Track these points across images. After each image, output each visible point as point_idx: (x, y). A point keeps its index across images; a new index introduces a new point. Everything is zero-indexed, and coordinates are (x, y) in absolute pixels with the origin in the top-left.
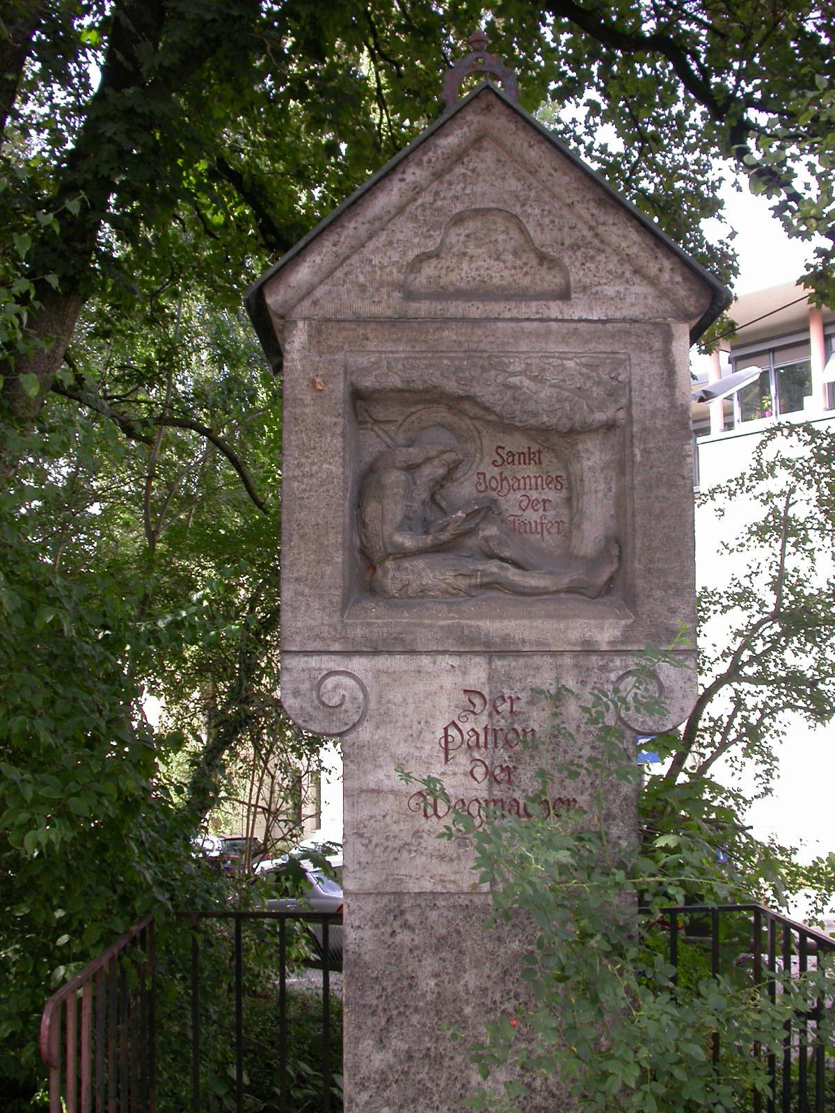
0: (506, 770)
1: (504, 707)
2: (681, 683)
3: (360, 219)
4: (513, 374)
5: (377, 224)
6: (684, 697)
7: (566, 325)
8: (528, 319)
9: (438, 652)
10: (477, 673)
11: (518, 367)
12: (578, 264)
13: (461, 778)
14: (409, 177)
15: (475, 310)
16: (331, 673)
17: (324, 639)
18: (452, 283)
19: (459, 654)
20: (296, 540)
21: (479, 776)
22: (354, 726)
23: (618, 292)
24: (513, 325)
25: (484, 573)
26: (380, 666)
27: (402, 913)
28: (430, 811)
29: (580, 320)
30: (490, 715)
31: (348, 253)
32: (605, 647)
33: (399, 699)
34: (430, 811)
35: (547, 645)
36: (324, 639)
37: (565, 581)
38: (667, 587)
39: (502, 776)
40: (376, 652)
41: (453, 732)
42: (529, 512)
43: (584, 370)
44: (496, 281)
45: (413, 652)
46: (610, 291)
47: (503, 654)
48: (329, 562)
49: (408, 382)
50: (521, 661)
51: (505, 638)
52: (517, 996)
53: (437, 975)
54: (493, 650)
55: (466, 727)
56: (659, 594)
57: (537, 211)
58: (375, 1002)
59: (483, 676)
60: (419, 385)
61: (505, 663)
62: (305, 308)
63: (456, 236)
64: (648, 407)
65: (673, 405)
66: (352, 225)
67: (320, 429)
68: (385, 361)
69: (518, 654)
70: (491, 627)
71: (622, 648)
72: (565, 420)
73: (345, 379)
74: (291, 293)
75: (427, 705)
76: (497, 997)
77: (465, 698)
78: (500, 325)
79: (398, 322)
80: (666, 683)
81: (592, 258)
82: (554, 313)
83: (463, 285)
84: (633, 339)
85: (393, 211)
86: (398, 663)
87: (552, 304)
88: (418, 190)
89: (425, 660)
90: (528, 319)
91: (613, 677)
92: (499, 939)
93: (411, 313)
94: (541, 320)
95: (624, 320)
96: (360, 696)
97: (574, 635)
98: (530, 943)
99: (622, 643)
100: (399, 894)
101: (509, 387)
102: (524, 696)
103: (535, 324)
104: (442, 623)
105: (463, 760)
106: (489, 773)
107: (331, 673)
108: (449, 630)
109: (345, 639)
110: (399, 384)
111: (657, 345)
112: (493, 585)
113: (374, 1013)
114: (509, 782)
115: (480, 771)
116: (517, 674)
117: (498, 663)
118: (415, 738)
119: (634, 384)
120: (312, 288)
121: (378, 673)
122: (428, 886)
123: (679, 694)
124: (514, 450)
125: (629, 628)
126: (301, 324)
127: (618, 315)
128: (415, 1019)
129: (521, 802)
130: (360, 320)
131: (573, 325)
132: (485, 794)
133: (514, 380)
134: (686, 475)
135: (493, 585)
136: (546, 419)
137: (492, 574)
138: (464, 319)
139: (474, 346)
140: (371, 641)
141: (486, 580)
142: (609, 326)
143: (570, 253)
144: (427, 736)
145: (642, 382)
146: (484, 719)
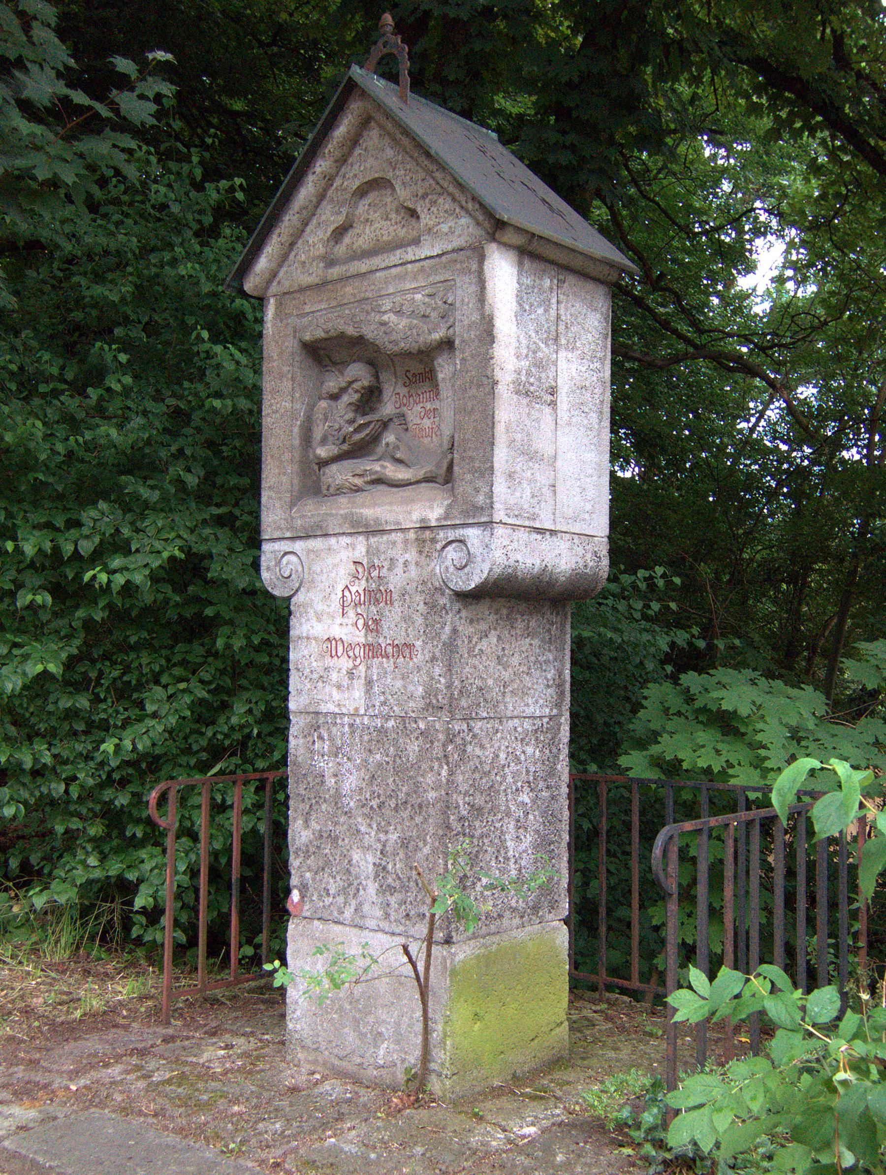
0: (376, 622)
1: (375, 574)
2: (481, 550)
3: (291, 212)
4: (385, 312)
5: (305, 212)
6: (483, 561)
7: (417, 264)
8: (395, 266)
9: (340, 534)
10: (360, 547)
11: (387, 306)
12: (426, 211)
13: (350, 627)
14: (318, 170)
15: (363, 266)
16: (286, 553)
17: (282, 529)
18: (360, 247)
19: (351, 534)
20: (269, 460)
21: (360, 627)
22: (297, 591)
23: (450, 227)
24: (385, 272)
25: (372, 472)
26: (310, 547)
27: (319, 727)
28: (334, 653)
29: (426, 258)
30: (367, 580)
31: (290, 240)
32: (434, 524)
33: (319, 570)
34: (334, 653)
35: (398, 523)
36: (282, 529)
37: (421, 474)
38: (473, 471)
39: (373, 626)
40: (308, 537)
41: (347, 593)
42: (426, 420)
43: (427, 300)
44: (385, 238)
45: (326, 535)
46: (445, 228)
47: (375, 533)
48: (285, 474)
49: (327, 332)
50: (385, 538)
51: (377, 520)
52: (379, 796)
53: (336, 775)
54: (372, 530)
55: (353, 589)
56: (468, 477)
57: (402, 172)
58: (304, 792)
59: (364, 550)
60: (332, 333)
61: (376, 539)
62: (274, 288)
63: (362, 207)
64: (466, 322)
65: (483, 315)
66: (287, 218)
67: (281, 376)
68: (320, 319)
69: (383, 532)
70: (369, 513)
71: (445, 523)
72: (414, 344)
73: (295, 337)
74: (258, 279)
75: (333, 575)
76: (368, 796)
77: (353, 567)
78: (378, 274)
79: (322, 285)
80: (472, 550)
81: (435, 202)
82: (410, 257)
83: (365, 247)
84: (458, 266)
85: (314, 200)
86: (316, 544)
87: (409, 249)
88: (329, 179)
89: (333, 540)
90: (395, 266)
91: (439, 547)
92: (370, 751)
93: (329, 278)
94: (401, 265)
95: (453, 251)
96: (300, 569)
97: (415, 516)
98: (387, 756)
99: (445, 519)
100: (317, 713)
101: (384, 324)
102: (386, 564)
103: (399, 269)
104: (342, 512)
105: (351, 614)
106: (366, 624)
107: (286, 553)
108: (345, 517)
109: (292, 528)
110: (323, 335)
111: (474, 267)
112: (379, 481)
113: (303, 801)
114: (377, 631)
115: (361, 622)
116: (382, 547)
117: (373, 540)
118: (326, 598)
119: (458, 304)
120: (274, 275)
121: (309, 551)
122: (332, 708)
123: (479, 559)
124: (416, 372)
125: (450, 506)
126: (272, 301)
127: (450, 248)
128: (324, 806)
129: (383, 645)
130: (302, 290)
131: (421, 263)
132: (362, 640)
133: (385, 318)
134: (489, 374)
135: (379, 481)
136: (403, 345)
137: (377, 472)
138: (359, 275)
139: (363, 295)
140: (304, 528)
141: (373, 477)
142: (444, 258)
143: (422, 202)
144: (333, 596)
145: (463, 300)
146: (363, 583)
